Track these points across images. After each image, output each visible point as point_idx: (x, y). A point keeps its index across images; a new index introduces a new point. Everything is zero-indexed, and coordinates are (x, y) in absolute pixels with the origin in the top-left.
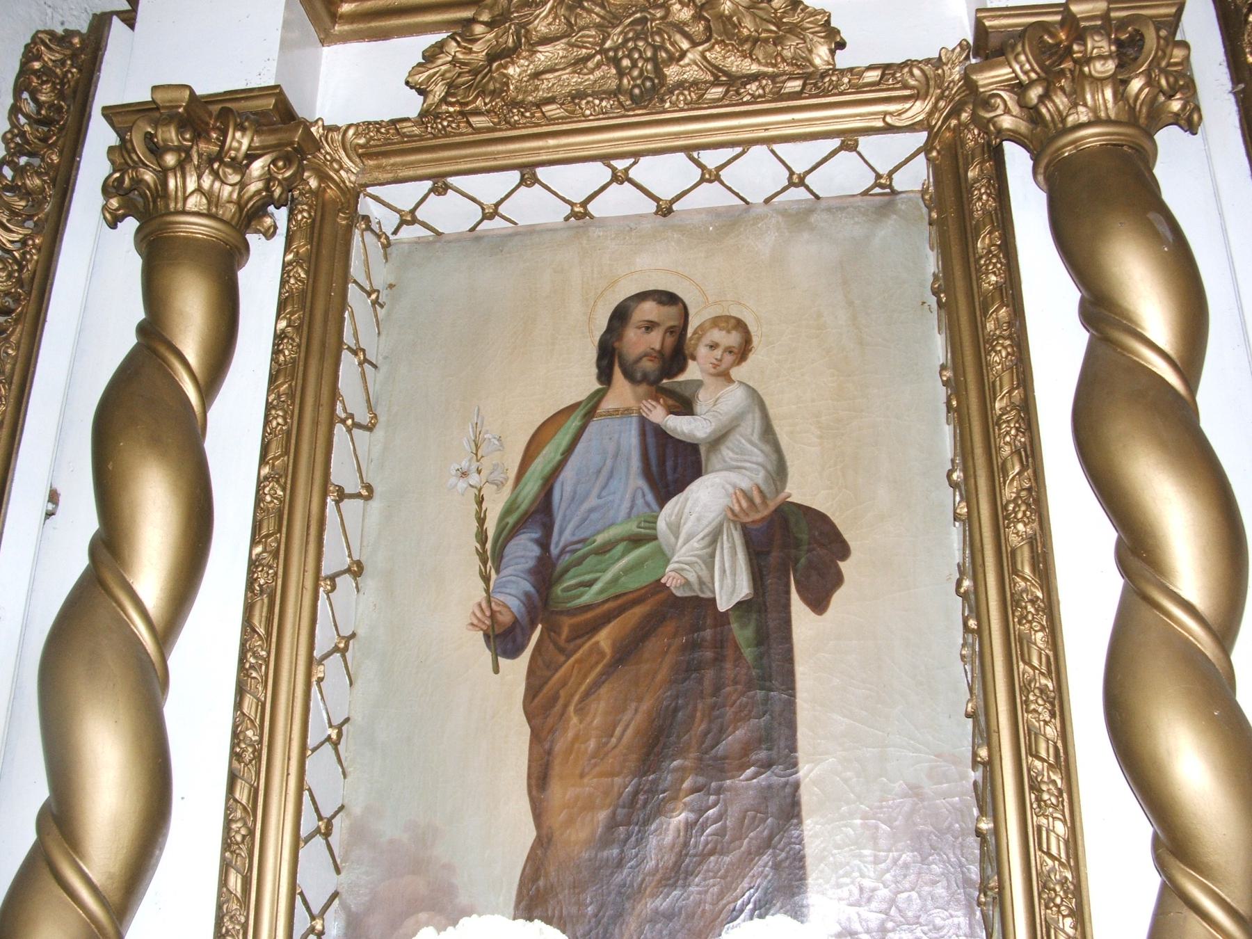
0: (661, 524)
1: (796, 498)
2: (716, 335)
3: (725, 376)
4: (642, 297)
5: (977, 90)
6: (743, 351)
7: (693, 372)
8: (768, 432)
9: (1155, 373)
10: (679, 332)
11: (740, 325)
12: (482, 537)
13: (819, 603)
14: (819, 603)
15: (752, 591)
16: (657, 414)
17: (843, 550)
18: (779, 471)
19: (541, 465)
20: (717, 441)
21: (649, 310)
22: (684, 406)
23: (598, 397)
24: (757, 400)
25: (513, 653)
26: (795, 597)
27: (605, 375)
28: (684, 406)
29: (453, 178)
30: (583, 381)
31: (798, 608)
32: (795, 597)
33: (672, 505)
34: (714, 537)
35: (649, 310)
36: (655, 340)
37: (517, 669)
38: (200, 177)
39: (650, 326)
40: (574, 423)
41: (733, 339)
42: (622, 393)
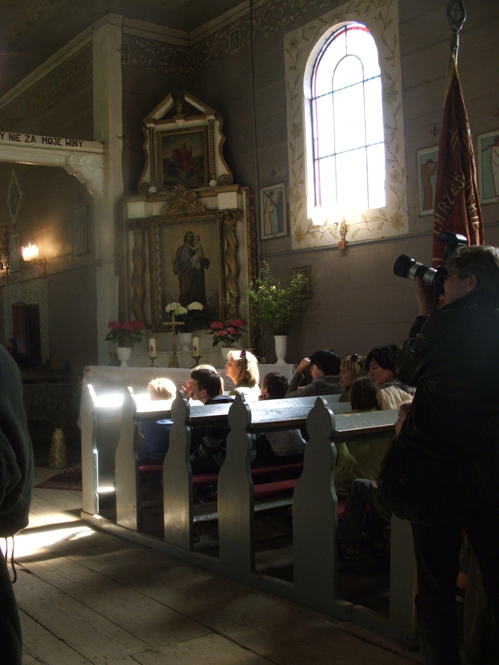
0: (191, 259)
1: (205, 257)
2: (196, 238)
3: (197, 243)
4: (188, 233)
5: (183, 105)
6: (199, 240)
7: (194, 242)
8: (202, 250)
9: (328, 395)
10: (192, 237)
11: (199, 237)
12: (173, 261)
13: (207, 269)
14: (207, 269)
15: (220, 210)
16: (190, 247)
17: (209, 263)
18: (203, 254)
19: (179, 253)
20: (197, 250)
21: (189, 234)
22: (193, 246)
23: (184, 245)
24: (200, 245)
25: (177, 274)
26: (205, 268)
27: (185, 243)
28: (193, 246)
29: (208, 199)
30: (182, 243)
31: (205, 269)
32: (205, 268)
33: (192, 258)
34: (197, 262)
35: (189, 234)
36: (190, 238)
37: (178, 276)
38: (193, 203)
39: (189, 236)
40: (182, 248)
41: (198, 238)
42: (187, 245)
